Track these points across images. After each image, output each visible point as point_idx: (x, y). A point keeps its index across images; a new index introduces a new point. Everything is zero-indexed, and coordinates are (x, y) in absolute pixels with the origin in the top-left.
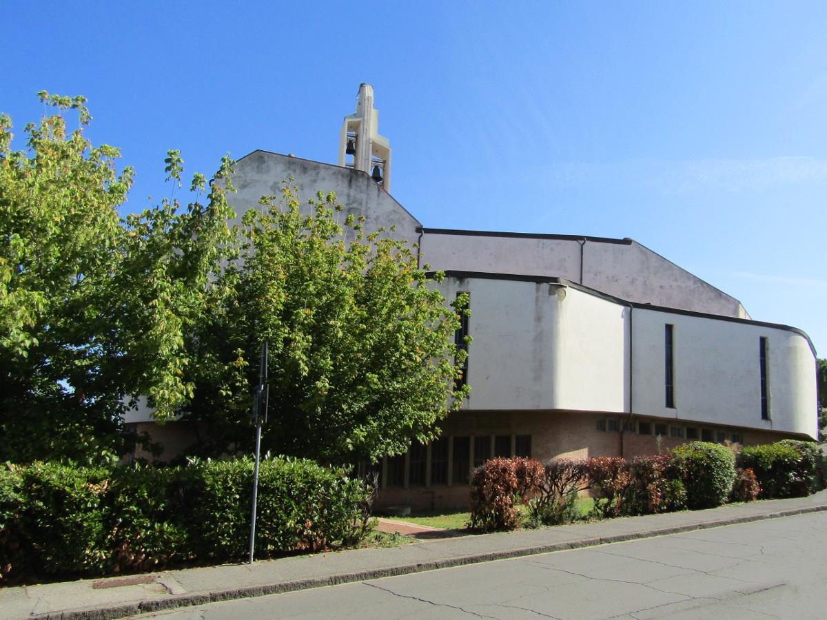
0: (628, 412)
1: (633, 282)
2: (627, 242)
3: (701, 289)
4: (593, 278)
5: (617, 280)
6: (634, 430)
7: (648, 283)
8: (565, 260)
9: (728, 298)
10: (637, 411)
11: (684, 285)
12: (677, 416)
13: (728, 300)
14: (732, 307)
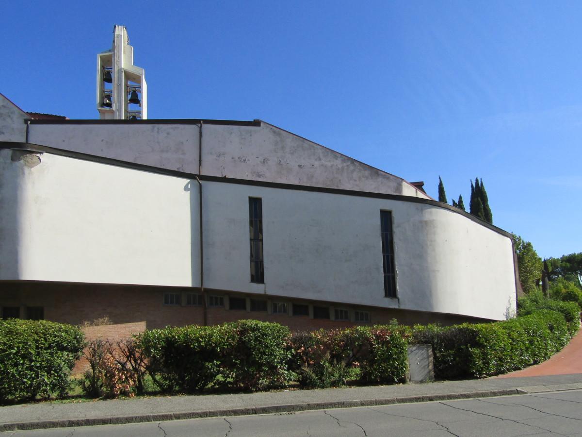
0: (199, 286)
1: (264, 162)
2: (257, 123)
3: (352, 168)
4: (217, 159)
5: (245, 160)
6: (222, 304)
7: (282, 162)
8: (182, 143)
9: (387, 176)
10: (215, 283)
11: (329, 164)
12: (265, 293)
13: (388, 178)
14: (393, 184)
